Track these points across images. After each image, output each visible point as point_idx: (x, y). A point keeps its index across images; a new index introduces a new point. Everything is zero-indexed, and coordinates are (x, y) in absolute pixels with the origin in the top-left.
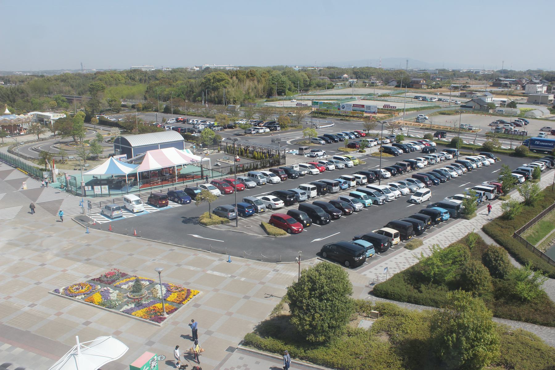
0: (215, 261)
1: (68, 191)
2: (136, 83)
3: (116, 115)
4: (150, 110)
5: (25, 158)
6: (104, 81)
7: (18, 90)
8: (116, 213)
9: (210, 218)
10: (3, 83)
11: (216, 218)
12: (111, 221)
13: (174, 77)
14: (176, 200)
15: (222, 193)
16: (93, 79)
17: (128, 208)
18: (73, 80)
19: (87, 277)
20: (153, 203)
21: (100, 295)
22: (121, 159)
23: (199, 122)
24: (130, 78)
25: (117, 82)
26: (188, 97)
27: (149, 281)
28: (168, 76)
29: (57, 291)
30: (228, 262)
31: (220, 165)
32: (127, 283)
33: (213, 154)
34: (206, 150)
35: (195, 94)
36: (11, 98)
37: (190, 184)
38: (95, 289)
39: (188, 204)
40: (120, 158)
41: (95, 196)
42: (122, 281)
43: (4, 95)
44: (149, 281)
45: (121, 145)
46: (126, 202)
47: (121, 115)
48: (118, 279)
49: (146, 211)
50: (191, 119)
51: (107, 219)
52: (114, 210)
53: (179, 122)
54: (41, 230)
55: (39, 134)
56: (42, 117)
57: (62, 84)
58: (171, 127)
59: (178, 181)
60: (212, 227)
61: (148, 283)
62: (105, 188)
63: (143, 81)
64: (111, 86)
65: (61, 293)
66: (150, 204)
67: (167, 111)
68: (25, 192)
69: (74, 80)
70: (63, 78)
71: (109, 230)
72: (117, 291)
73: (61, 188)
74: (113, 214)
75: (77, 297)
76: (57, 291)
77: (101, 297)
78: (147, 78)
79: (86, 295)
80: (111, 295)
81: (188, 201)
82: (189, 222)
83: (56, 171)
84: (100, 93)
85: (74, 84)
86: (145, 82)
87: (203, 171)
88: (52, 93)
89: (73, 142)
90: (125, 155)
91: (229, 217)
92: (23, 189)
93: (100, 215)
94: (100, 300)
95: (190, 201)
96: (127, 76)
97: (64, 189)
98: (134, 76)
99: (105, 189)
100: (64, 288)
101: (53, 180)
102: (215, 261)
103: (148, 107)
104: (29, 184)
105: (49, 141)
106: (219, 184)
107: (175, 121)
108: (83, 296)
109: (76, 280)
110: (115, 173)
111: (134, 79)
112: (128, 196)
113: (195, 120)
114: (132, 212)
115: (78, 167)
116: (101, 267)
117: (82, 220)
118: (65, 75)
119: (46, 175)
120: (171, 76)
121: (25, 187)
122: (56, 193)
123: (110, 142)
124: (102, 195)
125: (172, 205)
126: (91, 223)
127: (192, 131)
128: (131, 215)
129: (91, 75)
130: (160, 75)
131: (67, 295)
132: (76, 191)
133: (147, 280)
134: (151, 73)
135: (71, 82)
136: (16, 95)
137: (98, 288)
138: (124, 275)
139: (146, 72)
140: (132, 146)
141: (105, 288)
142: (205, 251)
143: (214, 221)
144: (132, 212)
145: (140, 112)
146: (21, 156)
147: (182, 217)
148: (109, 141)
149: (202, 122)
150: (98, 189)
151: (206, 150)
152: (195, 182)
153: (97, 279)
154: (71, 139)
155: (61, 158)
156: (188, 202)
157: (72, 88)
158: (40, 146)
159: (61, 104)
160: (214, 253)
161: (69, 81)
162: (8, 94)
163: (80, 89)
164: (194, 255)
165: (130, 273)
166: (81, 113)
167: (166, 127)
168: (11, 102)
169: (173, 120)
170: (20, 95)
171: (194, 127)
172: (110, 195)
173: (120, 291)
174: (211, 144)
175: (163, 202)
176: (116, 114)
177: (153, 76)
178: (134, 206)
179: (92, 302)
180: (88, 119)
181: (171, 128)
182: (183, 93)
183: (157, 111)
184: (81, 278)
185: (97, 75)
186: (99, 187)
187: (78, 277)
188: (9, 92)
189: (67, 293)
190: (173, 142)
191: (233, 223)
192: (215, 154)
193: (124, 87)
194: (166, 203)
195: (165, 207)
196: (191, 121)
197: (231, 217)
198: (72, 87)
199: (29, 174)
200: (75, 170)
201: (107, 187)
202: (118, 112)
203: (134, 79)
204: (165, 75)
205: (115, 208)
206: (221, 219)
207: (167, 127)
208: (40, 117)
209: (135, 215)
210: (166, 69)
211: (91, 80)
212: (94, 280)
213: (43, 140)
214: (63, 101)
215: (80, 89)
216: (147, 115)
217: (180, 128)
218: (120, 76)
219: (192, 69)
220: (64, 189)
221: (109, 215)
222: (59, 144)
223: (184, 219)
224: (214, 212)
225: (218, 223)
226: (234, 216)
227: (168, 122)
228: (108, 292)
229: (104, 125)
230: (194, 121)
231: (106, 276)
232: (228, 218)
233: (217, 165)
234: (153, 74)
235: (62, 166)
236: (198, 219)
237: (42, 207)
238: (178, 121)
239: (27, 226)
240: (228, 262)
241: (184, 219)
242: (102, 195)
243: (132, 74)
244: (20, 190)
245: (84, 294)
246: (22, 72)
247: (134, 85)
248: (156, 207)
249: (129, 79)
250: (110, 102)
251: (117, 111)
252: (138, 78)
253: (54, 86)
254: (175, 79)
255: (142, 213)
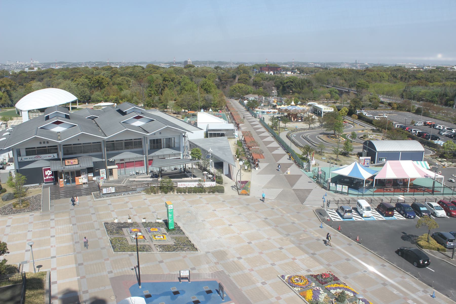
0: (420, 291)
1: (318, 183)
2: (397, 81)
3: (373, 111)
4: (404, 109)
5: (296, 145)
6: (371, 78)
7: (306, 80)
8: (348, 214)
9: (428, 242)
10: (299, 73)
11: (433, 242)
12: (342, 220)
13: (432, 77)
14: (402, 212)
15: (447, 215)
16: (363, 75)
17: (359, 211)
18: (346, 75)
19: (308, 271)
20: (381, 210)
21: (312, 293)
22: (365, 160)
23: (445, 129)
24: (393, 76)
25: (381, 79)
26: (441, 99)
27: (354, 293)
28: (426, 76)
29: (283, 277)
30: (431, 296)
31: (454, 181)
32: (336, 288)
33: (450, 167)
34: (445, 161)
35: (448, 97)
36: (301, 87)
37: (419, 197)
38: (310, 285)
39: (412, 220)
40: (365, 159)
41: (336, 192)
42: (332, 285)
43: (297, 84)
44: (354, 293)
45: (368, 147)
46: (358, 206)
47: (378, 111)
48: (330, 282)
49: (373, 218)
50: (439, 124)
51: (339, 217)
52: (346, 212)
53: (426, 125)
54: (289, 215)
55: (311, 124)
56: (317, 108)
57: (339, 77)
58: (418, 131)
59: (409, 192)
60: (427, 251)
61: (352, 295)
62: (345, 188)
63: (404, 80)
64: (375, 82)
65: (285, 280)
66: (379, 211)
67: (418, 112)
68: (288, 177)
69: (348, 75)
70: (340, 72)
71: (338, 229)
72: (326, 294)
73: (313, 178)
74: (345, 215)
75: (295, 289)
76: (283, 277)
77: (312, 295)
78: (407, 76)
79: (302, 289)
80: (320, 296)
81: (412, 217)
82: (407, 239)
83: (313, 162)
84: (364, 91)
85: (347, 78)
86: (405, 80)
87: (434, 187)
88: (330, 84)
89: (333, 135)
90: (370, 158)
91: (447, 246)
92: (287, 173)
93: (335, 212)
94: (310, 298)
95: (415, 217)
96: (391, 74)
97: (315, 180)
98: (397, 75)
99: (345, 189)
100: (289, 275)
101: (309, 170)
102: (420, 291)
103: (402, 107)
104: (293, 170)
105: (317, 130)
106: (446, 205)
107: (423, 124)
108: (300, 289)
109: (299, 271)
110: (354, 176)
111: (396, 77)
112: (361, 201)
113: (441, 126)
114: (361, 215)
115: (331, 161)
116: (321, 265)
117: (321, 213)
118: (341, 70)
119: (305, 165)
120: (429, 76)
121: (289, 172)
122: (309, 182)
123: (362, 139)
124: (342, 193)
125: (397, 216)
126: (326, 218)
127: (436, 138)
128: (359, 219)
129: (361, 71)
130: (419, 75)
131: (289, 284)
132: (324, 183)
133: (352, 292)
134: (412, 73)
135: (345, 77)
136: (304, 84)
137: (313, 285)
138: (336, 279)
139: (409, 70)
140: (377, 150)
141: (318, 288)
142: (412, 277)
143: (431, 246)
144: (361, 215)
145: (394, 111)
146: (294, 142)
147: (402, 232)
148: (362, 137)
149: (448, 129)
150: (340, 187)
151: (445, 161)
152: (425, 196)
153: (315, 276)
154: (332, 132)
155: (320, 150)
156: (412, 217)
157: (345, 81)
158: (308, 134)
159: (334, 95)
160: (421, 282)
161: (344, 75)
162: (300, 84)
163: (351, 83)
164: (401, 277)
165: (342, 279)
166: (345, 109)
167: (413, 130)
168: (300, 89)
169: (421, 123)
170: (307, 85)
171: (439, 133)
172: (348, 193)
173: (328, 295)
174: (450, 157)
175: (390, 213)
176: (374, 109)
177: (413, 75)
178: (363, 211)
179: (304, 297)
180: (350, 113)
181: (417, 132)
182: (436, 96)
183: (409, 111)
184: (304, 270)
185: (366, 72)
186: (341, 186)
187: (302, 269)
188: (300, 82)
189: (289, 282)
190: (408, 151)
191: (449, 254)
192: (452, 167)
193: (386, 84)
194: (392, 214)
195: (391, 218)
196: (437, 127)
197: (448, 246)
198: (345, 80)
199: (295, 161)
200: (328, 162)
201: (347, 187)
202: (376, 108)
203: (396, 77)
204: (424, 75)
205: (347, 210)
206: (438, 245)
207: (414, 131)
208: (315, 108)
209: (363, 219)
210: (427, 68)
211: (361, 76)
212: (312, 276)
213: (312, 129)
214: (336, 92)
215: (351, 83)
216: (399, 114)
217: (425, 133)
218: (385, 74)
219: (451, 68)
220: (315, 180)
221: (342, 214)
222: (323, 135)
223: (404, 235)
224: (433, 236)
225: (433, 249)
226: (452, 246)
227: (417, 124)
228: (318, 291)
229: (362, 120)
230: (440, 127)
231: (322, 276)
232: (445, 246)
233: (451, 181)
234: (413, 74)
235: (320, 157)
236: (416, 238)
237: (296, 194)
238: (425, 124)
239: (281, 209)
240: (431, 296)
241: (404, 235)
242: (342, 193)
243: (395, 73)
244: (285, 174)
245: (301, 288)
246: (314, 63)
247: (395, 83)
248: (382, 215)
249: (392, 76)
250: (371, 99)
251: (375, 107)
252: (399, 76)
253: (332, 78)
254: (433, 79)
255: (370, 218)
